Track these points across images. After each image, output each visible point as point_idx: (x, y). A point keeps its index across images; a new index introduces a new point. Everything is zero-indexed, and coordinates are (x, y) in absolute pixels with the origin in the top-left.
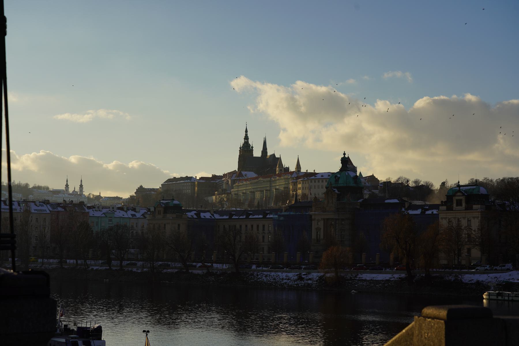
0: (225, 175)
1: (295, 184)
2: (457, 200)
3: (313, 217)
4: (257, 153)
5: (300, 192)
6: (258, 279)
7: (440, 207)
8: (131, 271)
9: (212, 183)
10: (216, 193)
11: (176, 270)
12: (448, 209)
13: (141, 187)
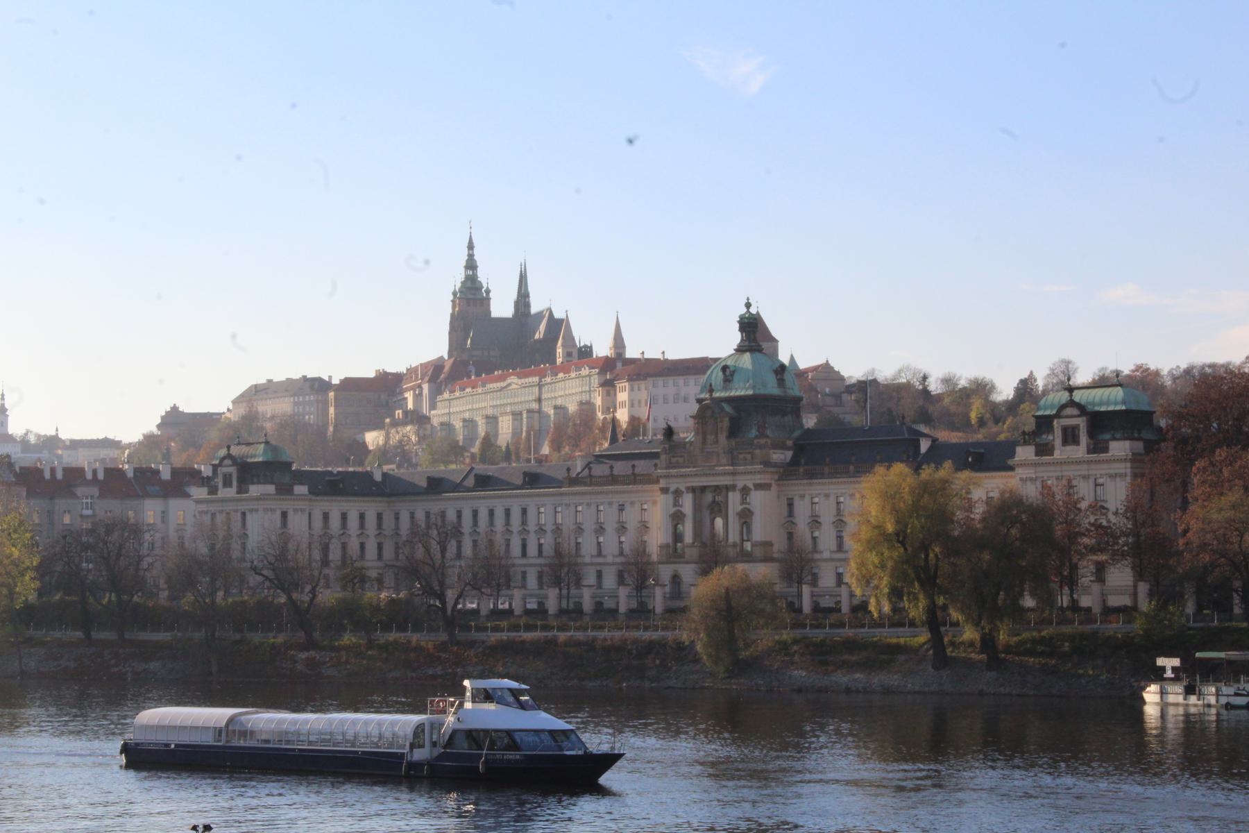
2: (1065, 430)
4: (502, 307)
5: (622, 416)
13: (873, 371)
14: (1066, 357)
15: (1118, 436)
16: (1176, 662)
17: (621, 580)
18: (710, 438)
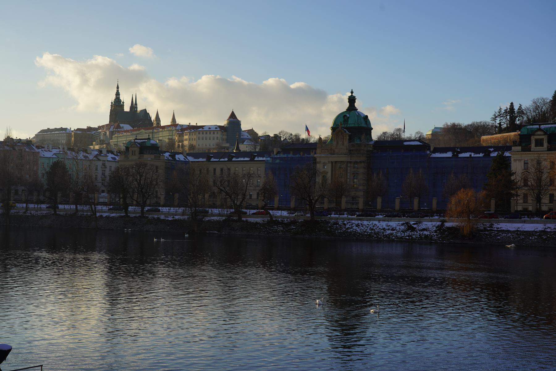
0: (100, 127)
1: (181, 135)
2: (536, 140)
3: (318, 160)
4: (127, 109)
5: (186, 143)
6: (348, 228)
8: (158, 218)
9: (86, 135)
10: (94, 143)
11: (224, 218)
12: (523, 150)
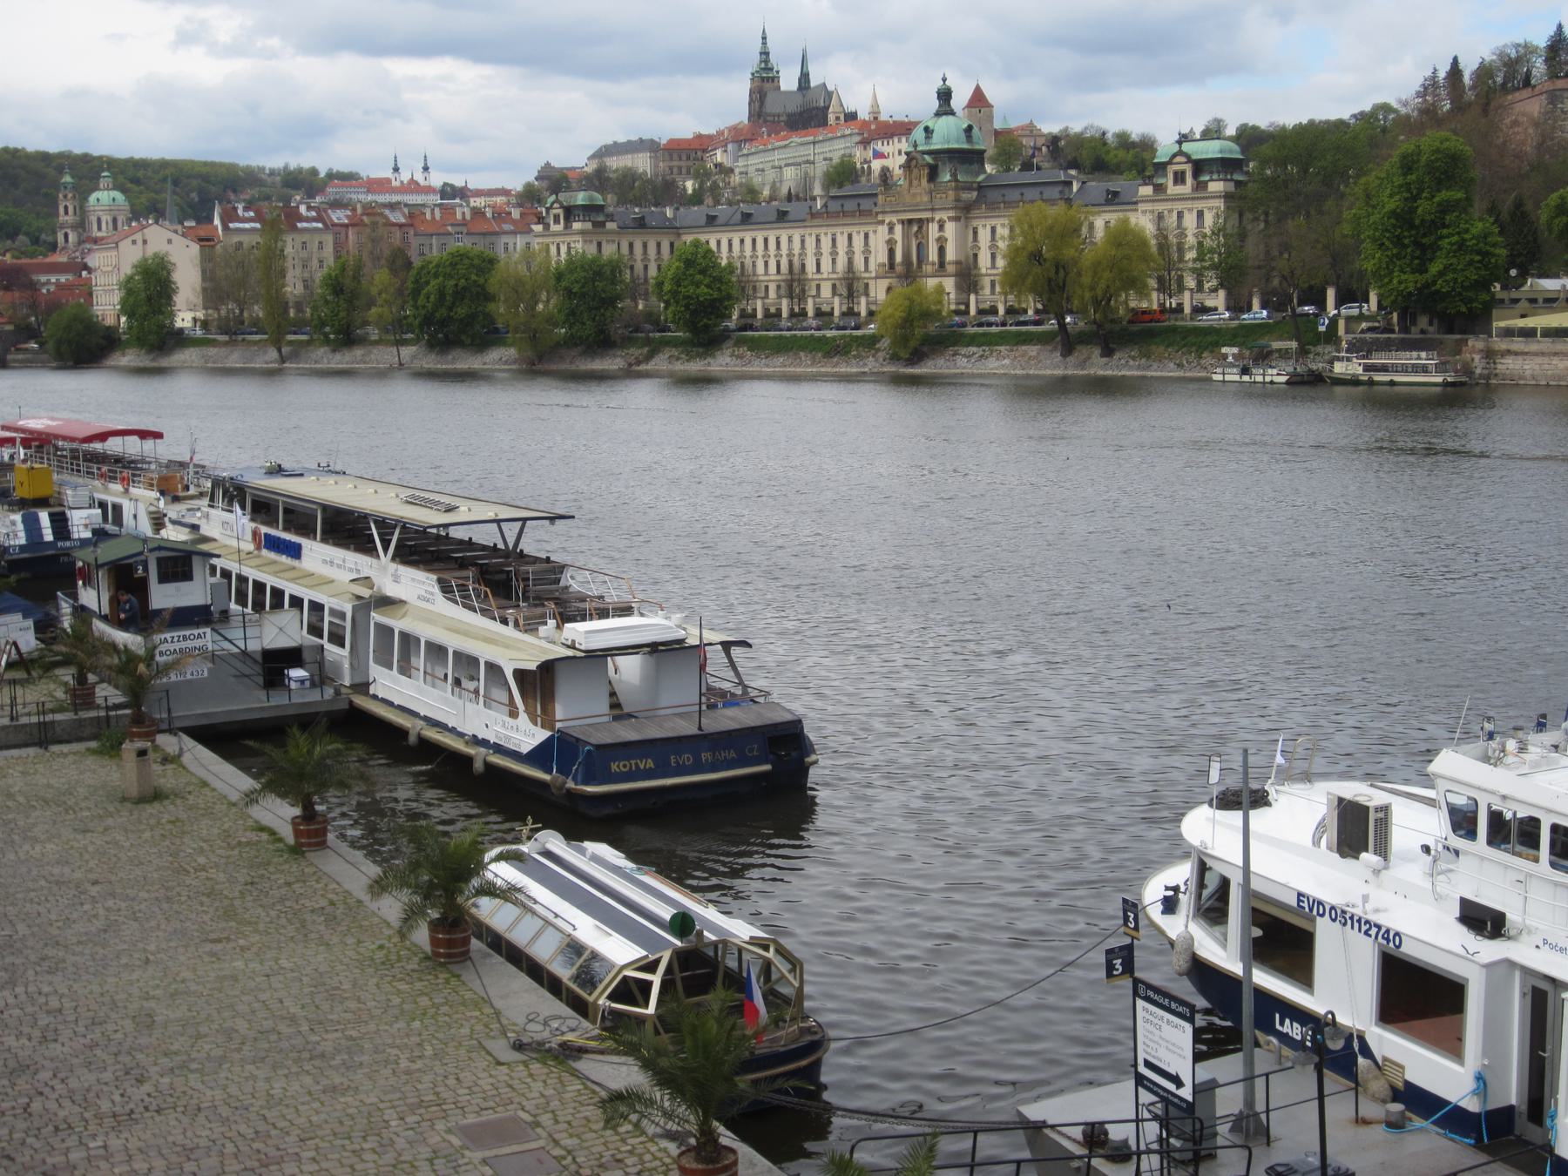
2: (1176, 173)
4: (788, 81)
7: (667, 917)
13: (548, 164)
14: (1219, 116)
15: (1215, 176)
16: (1235, 350)
17: (834, 292)
18: (915, 183)
